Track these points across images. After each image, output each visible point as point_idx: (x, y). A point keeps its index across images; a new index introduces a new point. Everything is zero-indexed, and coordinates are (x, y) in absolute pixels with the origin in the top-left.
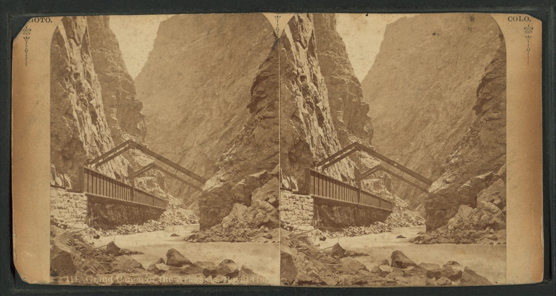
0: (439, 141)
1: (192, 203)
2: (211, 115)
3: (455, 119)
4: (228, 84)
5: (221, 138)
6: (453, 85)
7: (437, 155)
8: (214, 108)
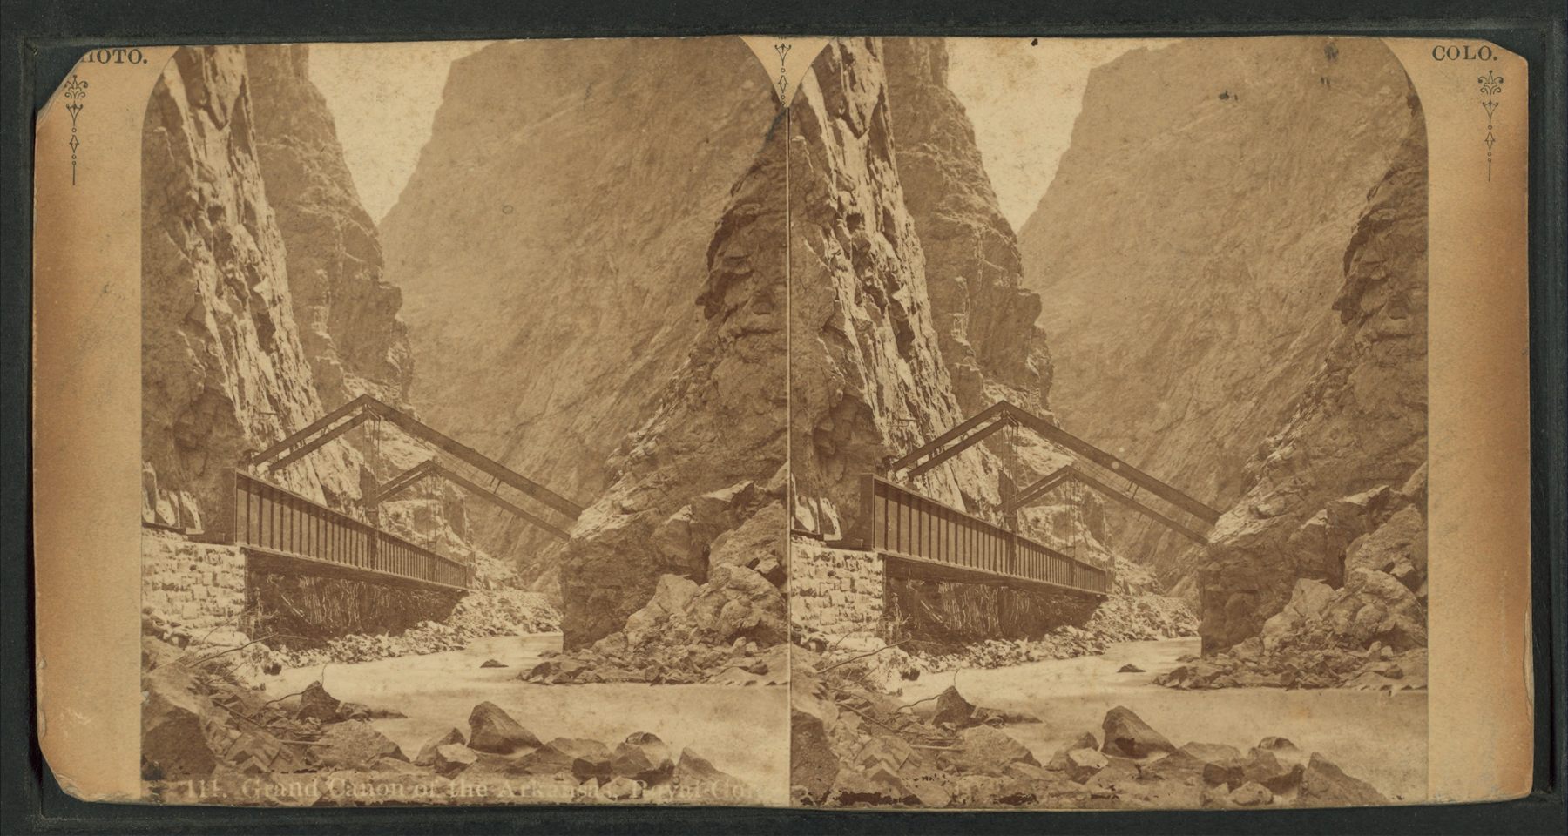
0: (1238, 398)
1: (540, 573)
3: (1282, 335)
4: (643, 237)
5: (625, 391)
6: (1278, 240)
7: (1232, 438)
8: (604, 304)
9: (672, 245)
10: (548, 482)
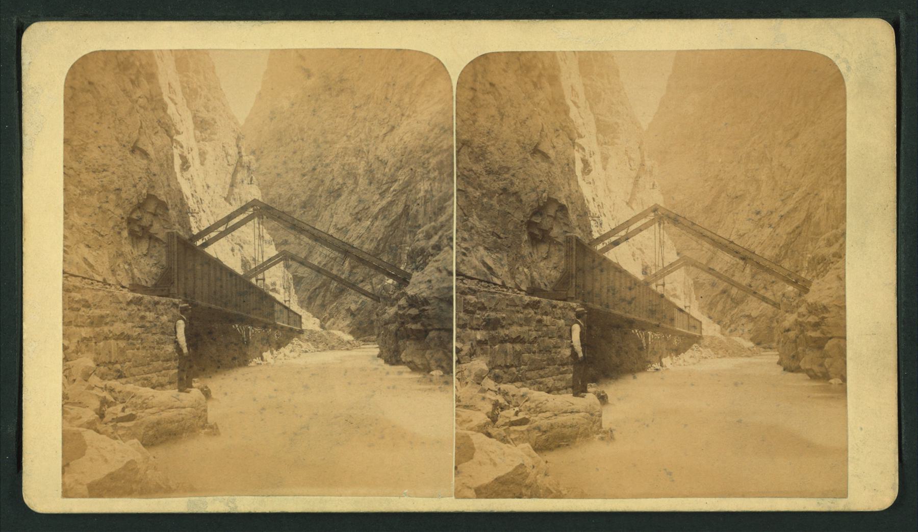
0: (360, 220)
1: (329, 319)
3: (386, 183)
4: (384, 131)
10: (733, 276)
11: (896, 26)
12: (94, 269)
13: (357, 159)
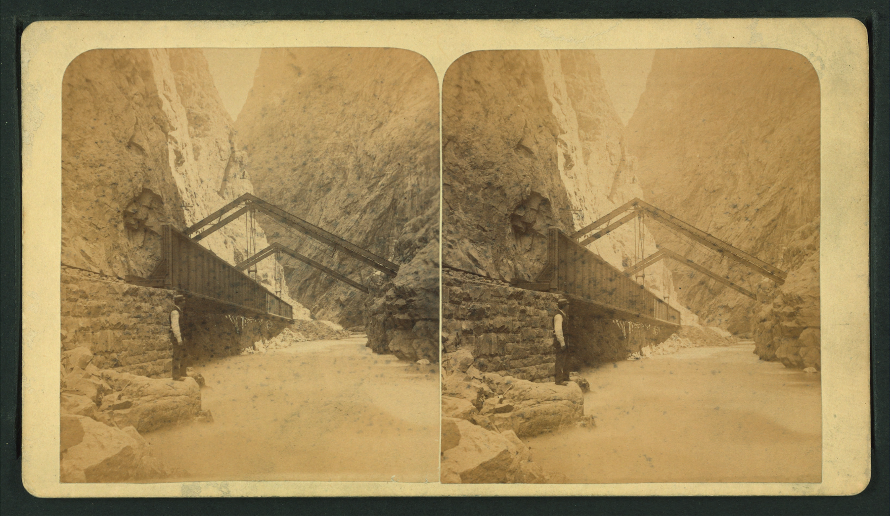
0: (349, 213)
2: (735, 183)
3: (374, 178)
4: (372, 127)
8: (740, 172)
9: (389, 131)
11: (869, 25)
12: (91, 261)
13: (346, 154)
